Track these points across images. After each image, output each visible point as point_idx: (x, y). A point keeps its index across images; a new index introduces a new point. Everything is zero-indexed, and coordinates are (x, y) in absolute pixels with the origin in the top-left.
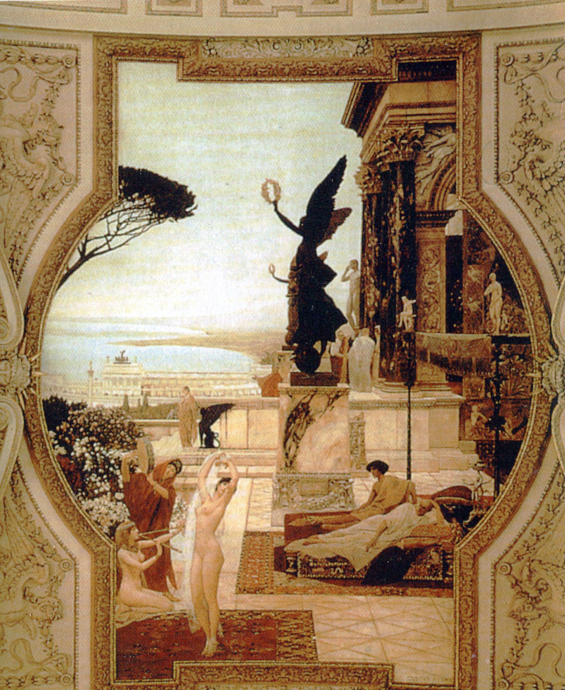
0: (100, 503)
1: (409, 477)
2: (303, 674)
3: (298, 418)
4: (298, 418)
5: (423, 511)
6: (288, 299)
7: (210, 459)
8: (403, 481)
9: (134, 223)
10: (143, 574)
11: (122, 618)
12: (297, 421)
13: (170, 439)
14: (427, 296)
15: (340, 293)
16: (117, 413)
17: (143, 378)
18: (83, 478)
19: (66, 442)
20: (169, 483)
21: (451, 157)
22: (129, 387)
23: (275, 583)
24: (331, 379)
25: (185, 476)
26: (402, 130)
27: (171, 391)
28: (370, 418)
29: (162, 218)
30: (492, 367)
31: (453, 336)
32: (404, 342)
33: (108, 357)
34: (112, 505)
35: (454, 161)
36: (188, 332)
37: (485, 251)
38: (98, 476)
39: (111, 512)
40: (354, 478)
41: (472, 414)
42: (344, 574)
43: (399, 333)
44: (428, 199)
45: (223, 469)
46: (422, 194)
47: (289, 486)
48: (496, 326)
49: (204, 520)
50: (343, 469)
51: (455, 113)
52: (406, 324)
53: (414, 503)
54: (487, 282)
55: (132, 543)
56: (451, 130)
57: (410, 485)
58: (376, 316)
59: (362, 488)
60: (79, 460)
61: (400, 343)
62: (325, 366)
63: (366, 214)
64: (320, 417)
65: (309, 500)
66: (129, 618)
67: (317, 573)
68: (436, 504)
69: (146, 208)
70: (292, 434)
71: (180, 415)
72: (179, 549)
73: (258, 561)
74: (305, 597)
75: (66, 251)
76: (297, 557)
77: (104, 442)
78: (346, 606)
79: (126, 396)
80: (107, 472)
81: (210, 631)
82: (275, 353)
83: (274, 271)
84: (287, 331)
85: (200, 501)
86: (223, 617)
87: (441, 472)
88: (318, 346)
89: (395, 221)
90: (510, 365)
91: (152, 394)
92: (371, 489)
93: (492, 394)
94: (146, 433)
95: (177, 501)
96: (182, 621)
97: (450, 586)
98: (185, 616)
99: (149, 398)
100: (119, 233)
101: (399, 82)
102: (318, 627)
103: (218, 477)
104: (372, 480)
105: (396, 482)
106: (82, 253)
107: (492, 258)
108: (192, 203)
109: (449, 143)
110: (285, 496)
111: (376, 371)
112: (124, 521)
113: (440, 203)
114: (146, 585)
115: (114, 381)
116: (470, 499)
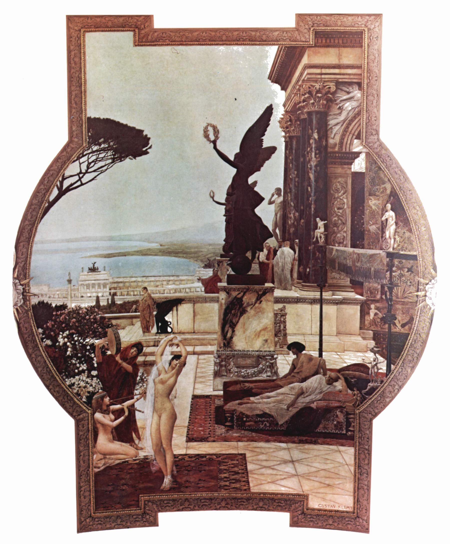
0: (80, 379)
1: (321, 355)
2: (239, 503)
3: (232, 315)
4: (232, 315)
5: (331, 381)
6: (225, 218)
7: (165, 341)
8: (316, 358)
9: (100, 162)
10: (114, 431)
11: (98, 463)
12: (233, 312)
13: (133, 327)
14: (336, 218)
15: (267, 213)
16: (91, 310)
17: (111, 283)
18: (66, 362)
19: (51, 335)
20: (133, 361)
21: (357, 110)
22: (99, 290)
23: (217, 433)
24: (261, 279)
25: (145, 355)
26: (317, 86)
27: (134, 291)
28: (290, 309)
29: (123, 157)
30: (387, 276)
31: (357, 250)
32: (318, 253)
33: (82, 268)
34: (89, 380)
35: (359, 114)
36: (146, 245)
37: (383, 186)
38: (77, 359)
39: (88, 386)
40: (277, 354)
41: (371, 311)
42: (269, 427)
43: (313, 246)
44: (338, 142)
45: (175, 349)
46: (333, 138)
47: (227, 360)
48: (390, 244)
49: (160, 387)
50: (269, 348)
51: (361, 75)
52: (319, 239)
53: (325, 374)
54: (384, 210)
55: (105, 408)
56: (357, 88)
57: (322, 362)
58: (295, 233)
59: (284, 363)
60: (62, 348)
61: (314, 254)
62: (255, 269)
63: (287, 152)
64: (251, 308)
65: (243, 371)
66: (104, 464)
67: (249, 426)
68: (341, 376)
69: (110, 150)
70: (229, 322)
71: (140, 309)
72: (142, 410)
73: (203, 417)
74: (240, 443)
75: (48, 190)
76: (233, 414)
77: (80, 334)
78: (272, 450)
79: (98, 297)
80: (84, 356)
81: (166, 470)
82: (215, 259)
83: (214, 196)
84: (224, 243)
85: (157, 373)
86: (177, 459)
87: (346, 352)
88: (249, 255)
89: (312, 158)
90: (401, 276)
91: (118, 294)
92: (291, 363)
93: (386, 296)
94: (114, 324)
95: (140, 374)
96: (145, 463)
97: (352, 438)
98: (148, 460)
99: (115, 297)
100: (89, 170)
101: (315, 46)
102: (250, 467)
103: (172, 354)
104: (292, 357)
105: (310, 358)
106: (60, 189)
107: (388, 192)
108: (148, 144)
109: (355, 98)
110: (224, 368)
111: (295, 275)
112: (98, 392)
113: (348, 146)
114: (117, 439)
115: (88, 286)
116: (368, 374)
